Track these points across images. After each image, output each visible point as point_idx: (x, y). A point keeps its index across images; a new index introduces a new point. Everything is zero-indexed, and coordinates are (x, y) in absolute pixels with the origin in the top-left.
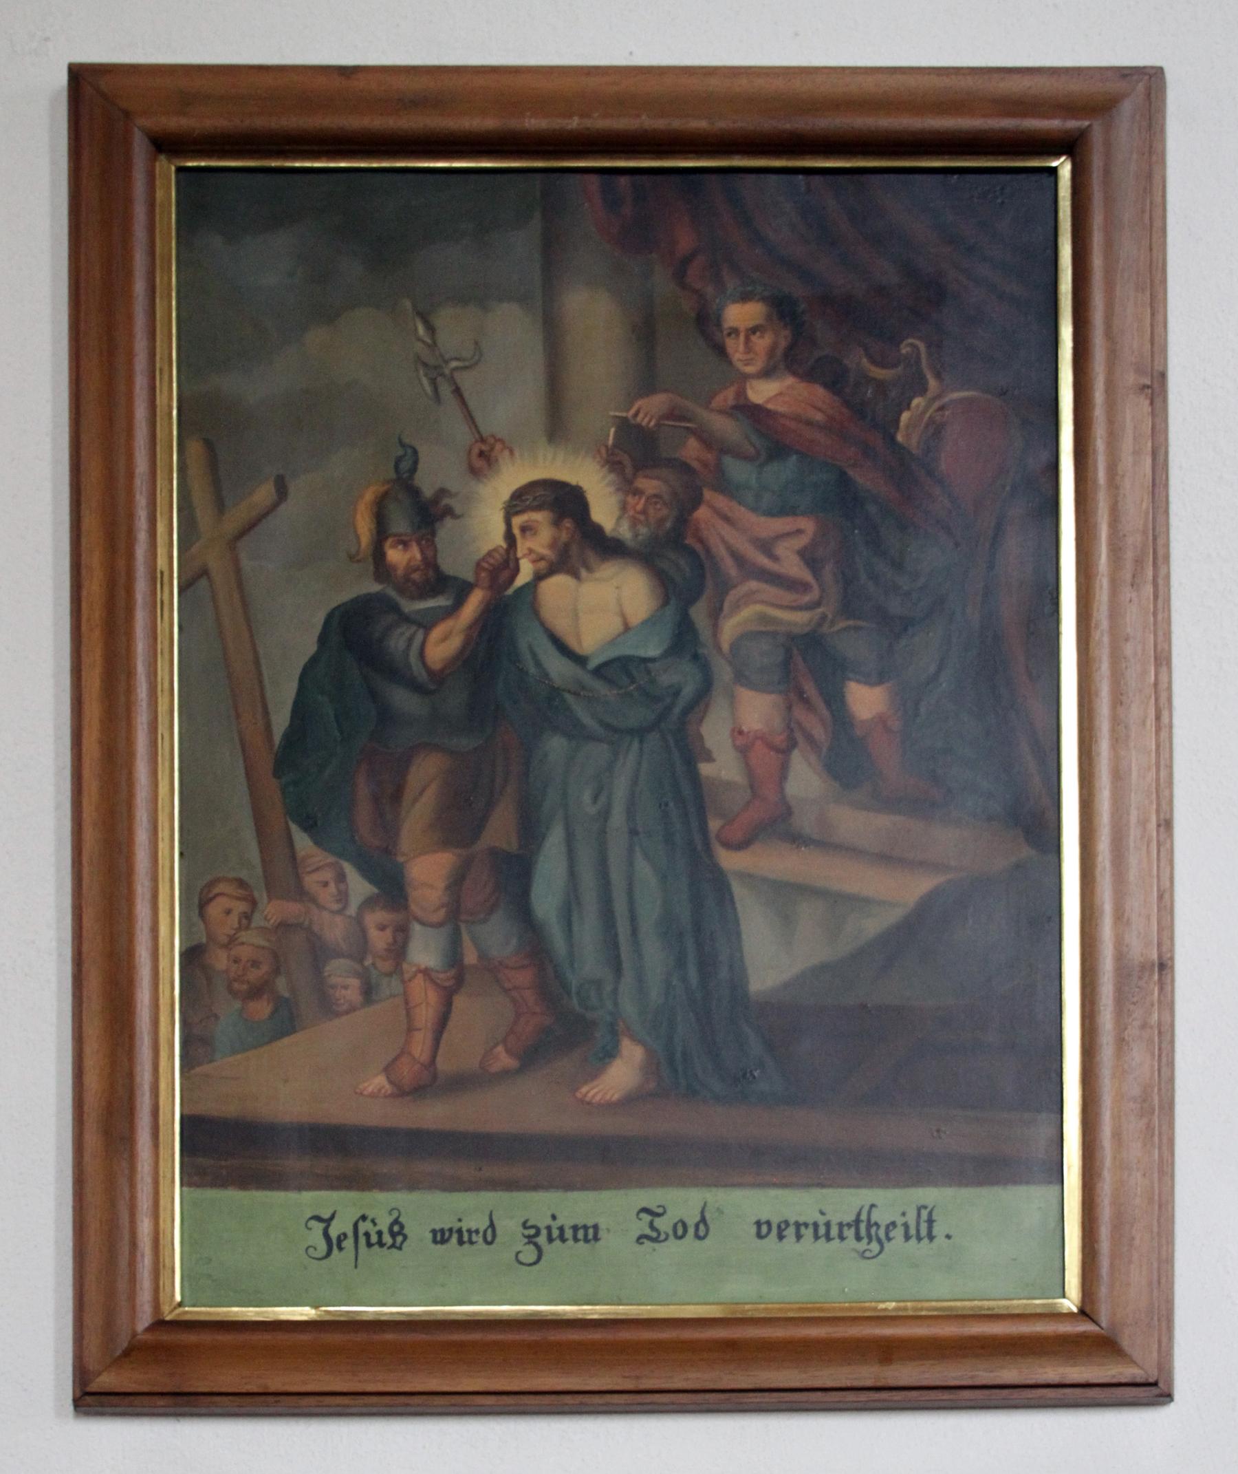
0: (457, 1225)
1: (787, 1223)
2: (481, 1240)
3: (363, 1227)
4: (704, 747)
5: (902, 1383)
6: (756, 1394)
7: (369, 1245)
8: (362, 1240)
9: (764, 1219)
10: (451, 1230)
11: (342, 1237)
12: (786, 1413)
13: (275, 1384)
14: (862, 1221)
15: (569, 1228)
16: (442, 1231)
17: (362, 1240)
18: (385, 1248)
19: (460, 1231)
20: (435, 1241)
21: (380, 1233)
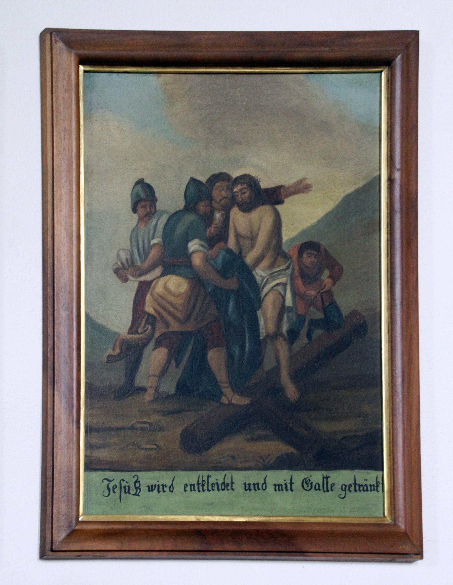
0: (157, 484)
2: (168, 490)
3: (124, 484)
4: (333, 280)
9: (256, 483)
10: (155, 486)
11: (115, 487)
14: (200, 484)
16: (152, 486)
18: (130, 495)
19: (217, 483)
20: (149, 491)
21: (286, 484)
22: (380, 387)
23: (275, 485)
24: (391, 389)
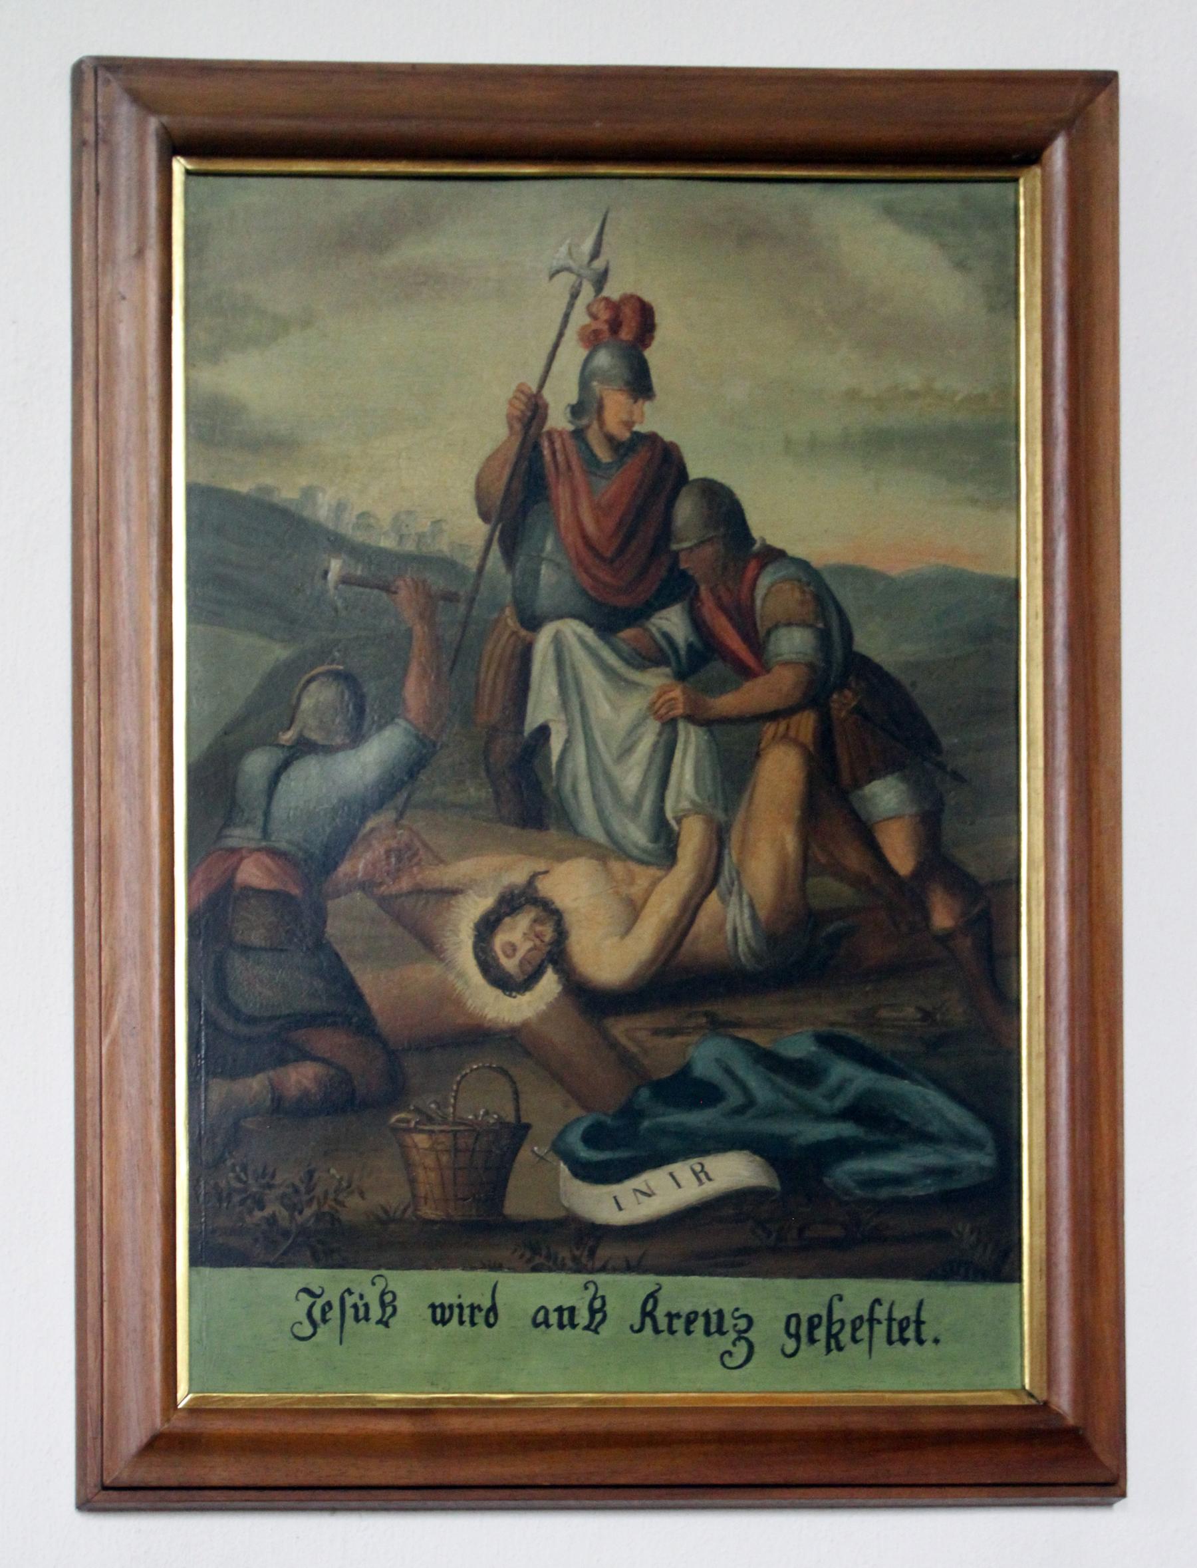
0: (455, 1301)
1: (696, 1313)
3: (350, 1300)
5: (375, 1482)
6: (301, 1493)
7: (357, 1319)
8: (350, 1312)
12: (1073, 1507)
13: (1053, 1478)
14: (879, 1322)
15: (351, 1307)
17: (350, 1312)
22: (1014, 746)
23: (433, 1307)
24: (564, 805)
